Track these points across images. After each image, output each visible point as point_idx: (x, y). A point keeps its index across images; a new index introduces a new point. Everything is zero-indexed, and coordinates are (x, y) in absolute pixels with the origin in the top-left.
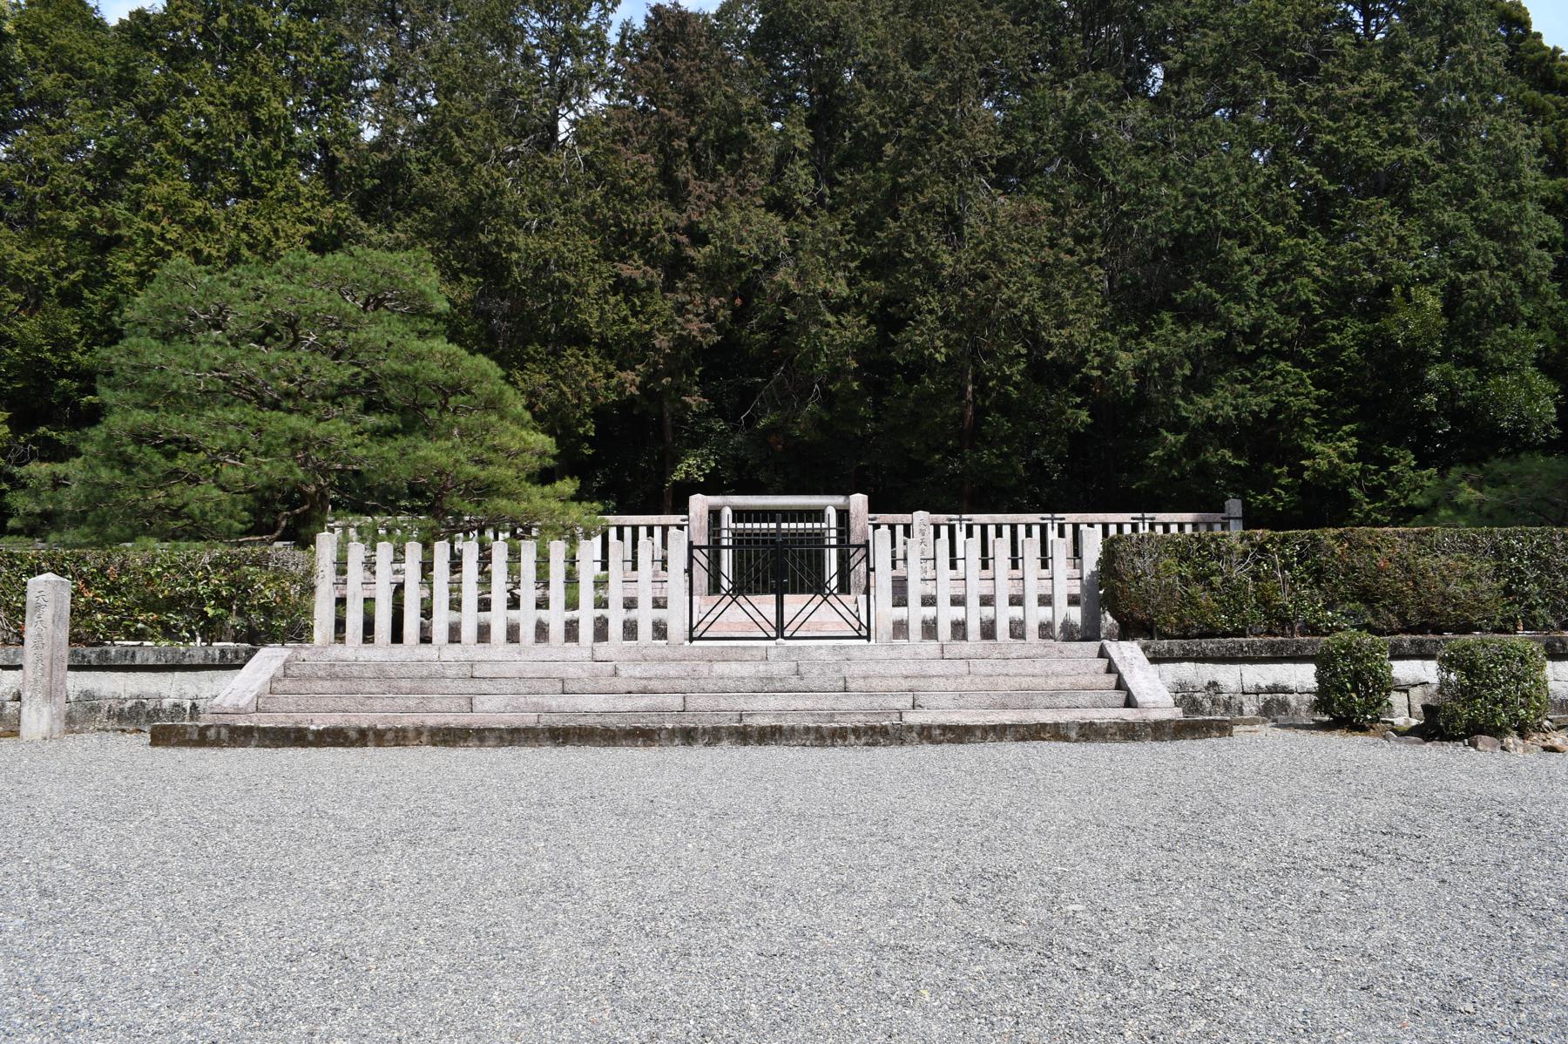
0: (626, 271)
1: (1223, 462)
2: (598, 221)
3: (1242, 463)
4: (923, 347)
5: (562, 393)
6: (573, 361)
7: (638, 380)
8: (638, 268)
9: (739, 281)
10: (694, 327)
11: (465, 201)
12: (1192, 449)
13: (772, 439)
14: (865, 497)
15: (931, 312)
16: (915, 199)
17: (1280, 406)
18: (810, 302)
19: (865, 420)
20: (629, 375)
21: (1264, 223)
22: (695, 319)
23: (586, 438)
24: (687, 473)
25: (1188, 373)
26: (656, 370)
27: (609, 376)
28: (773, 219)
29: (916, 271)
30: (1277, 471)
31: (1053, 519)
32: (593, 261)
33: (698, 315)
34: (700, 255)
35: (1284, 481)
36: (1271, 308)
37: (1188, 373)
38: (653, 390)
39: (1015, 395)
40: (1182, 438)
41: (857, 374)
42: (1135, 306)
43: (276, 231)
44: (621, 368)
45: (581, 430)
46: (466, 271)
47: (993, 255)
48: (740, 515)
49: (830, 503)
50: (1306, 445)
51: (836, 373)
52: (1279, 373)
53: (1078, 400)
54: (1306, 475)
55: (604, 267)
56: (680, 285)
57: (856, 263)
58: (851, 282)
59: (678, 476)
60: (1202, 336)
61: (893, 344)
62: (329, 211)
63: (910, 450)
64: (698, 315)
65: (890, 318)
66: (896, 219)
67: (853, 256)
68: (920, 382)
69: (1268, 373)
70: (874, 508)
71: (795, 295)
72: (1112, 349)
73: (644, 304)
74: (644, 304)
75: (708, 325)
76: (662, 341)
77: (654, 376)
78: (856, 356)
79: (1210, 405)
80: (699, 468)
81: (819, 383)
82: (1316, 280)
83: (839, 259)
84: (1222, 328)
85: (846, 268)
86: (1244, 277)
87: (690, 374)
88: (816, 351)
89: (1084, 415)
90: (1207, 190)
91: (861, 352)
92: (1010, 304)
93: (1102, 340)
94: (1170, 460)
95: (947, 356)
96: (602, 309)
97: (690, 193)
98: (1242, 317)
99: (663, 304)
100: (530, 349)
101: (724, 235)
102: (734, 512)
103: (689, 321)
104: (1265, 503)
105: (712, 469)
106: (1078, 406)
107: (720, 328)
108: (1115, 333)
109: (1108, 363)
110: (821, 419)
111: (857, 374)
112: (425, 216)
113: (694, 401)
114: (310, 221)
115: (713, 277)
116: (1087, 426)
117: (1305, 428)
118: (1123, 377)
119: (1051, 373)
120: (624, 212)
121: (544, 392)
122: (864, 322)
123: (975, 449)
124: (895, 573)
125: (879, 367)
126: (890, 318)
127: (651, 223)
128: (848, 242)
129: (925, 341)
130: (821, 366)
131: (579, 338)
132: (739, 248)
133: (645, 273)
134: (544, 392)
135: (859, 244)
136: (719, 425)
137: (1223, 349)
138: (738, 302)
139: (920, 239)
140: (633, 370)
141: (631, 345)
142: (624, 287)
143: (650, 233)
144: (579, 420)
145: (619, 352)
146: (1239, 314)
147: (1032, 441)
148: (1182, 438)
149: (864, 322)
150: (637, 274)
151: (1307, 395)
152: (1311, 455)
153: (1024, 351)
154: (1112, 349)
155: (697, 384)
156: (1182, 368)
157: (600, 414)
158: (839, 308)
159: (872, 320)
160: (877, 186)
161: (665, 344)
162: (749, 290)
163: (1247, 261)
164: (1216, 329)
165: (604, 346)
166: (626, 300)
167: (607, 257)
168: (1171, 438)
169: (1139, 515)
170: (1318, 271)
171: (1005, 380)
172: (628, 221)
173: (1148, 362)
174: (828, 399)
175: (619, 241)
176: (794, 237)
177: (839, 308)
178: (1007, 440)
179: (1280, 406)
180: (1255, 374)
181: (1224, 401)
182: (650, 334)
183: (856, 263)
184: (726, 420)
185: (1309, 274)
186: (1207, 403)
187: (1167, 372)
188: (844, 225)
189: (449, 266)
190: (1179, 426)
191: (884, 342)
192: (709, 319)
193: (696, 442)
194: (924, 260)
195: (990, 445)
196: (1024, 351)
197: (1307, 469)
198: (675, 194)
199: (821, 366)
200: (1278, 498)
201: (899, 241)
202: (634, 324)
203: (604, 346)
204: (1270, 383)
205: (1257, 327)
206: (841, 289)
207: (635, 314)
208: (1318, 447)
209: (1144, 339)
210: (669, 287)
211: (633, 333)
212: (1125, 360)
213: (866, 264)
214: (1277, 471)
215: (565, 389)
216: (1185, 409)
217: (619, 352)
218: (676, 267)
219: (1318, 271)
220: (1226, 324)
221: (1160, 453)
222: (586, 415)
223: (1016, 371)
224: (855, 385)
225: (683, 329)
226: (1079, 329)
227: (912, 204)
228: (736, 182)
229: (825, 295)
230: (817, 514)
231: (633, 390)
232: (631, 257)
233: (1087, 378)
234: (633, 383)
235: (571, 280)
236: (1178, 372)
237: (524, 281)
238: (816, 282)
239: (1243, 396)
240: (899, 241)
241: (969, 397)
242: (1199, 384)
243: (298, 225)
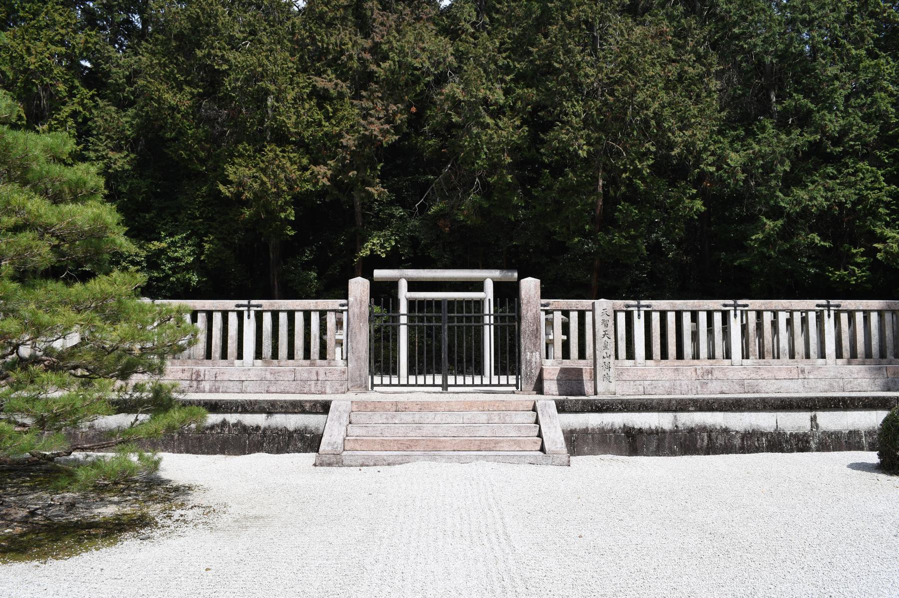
0: (320, 83)
1: (812, 245)
2: (297, 42)
3: (827, 244)
4: (568, 143)
5: (263, 183)
6: (271, 155)
7: (329, 173)
8: (330, 81)
9: (414, 90)
10: (376, 128)
11: (186, 24)
12: (786, 234)
13: (441, 223)
14: (538, 281)
15: (576, 115)
16: (563, 18)
17: (862, 199)
18: (472, 106)
19: (517, 207)
20: (322, 169)
21: (849, 47)
22: (373, 121)
23: (287, 221)
24: (371, 250)
25: (788, 169)
26: (344, 166)
27: (304, 169)
28: (444, 40)
29: (564, 79)
30: (854, 251)
31: (735, 306)
32: (292, 74)
33: (379, 119)
34: (381, 70)
35: (859, 260)
36: (856, 118)
37: (788, 169)
38: (342, 181)
39: (642, 187)
40: (780, 223)
41: (511, 168)
42: (742, 118)
43: (28, 49)
44: (316, 164)
45: (283, 215)
46: (189, 83)
47: (629, 67)
48: (414, 286)
49: (489, 276)
50: (879, 231)
51: (494, 167)
52: (860, 170)
53: (694, 191)
54: (879, 256)
55: (301, 79)
56: (364, 93)
57: (511, 76)
58: (507, 92)
59: (365, 253)
60: (800, 139)
61: (543, 142)
62: (81, 37)
63: (555, 233)
64: (379, 119)
65: (539, 121)
66: (546, 36)
67: (507, 69)
68: (565, 175)
69: (851, 170)
70: (546, 293)
71: (460, 101)
72: (723, 149)
73: (335, 111)
74: (334, 112)
75: (387, 126)
76: (349, 140)
77: (344, 169)
78: (511, 153)
79: (806, 197)
80: (382, 246)
81: (480, 177)
82: (891, 95)
83: (495, 73)
84: (816, 132)
85: (502, 81)
86: (834, 91)
87: (373, 169)
88: (477, 150)
89: (699, 205)
90: (806, 15)
91: (515, 149)
92: (644, 106)
93: (715, 142)
94: (767, 242)
95: (588, 152)
96: (298, 112)
97: (374, 20)
98: (833, 123)
99: (350, 111)
100: (240, 147)
101: (401, 51)
102: (408, 282)
103: (371, 123)
104: (842, 278)
105: (393, 247)
106: (693, 198)
107: (397, 130)
108: (724, 136)
109: (720, 162)
110: (481, 207)
111: (511, 168)
112: (157, 39)
113: (376, 190)
114: (62, 43)
115: (392, 89)
116: (700, 215)
117: (877, 216)
118: (732, 173)
119: (672, 170)
120: (319, 34)
121: (249, 181)
122: (518, 123)
123: (607, 232)
124: (567, 364)
125: (529, 163)
126: (539, 121)
127: (342, 44)
128: (505, 58)
129: (570, 139)
130: (481, 162)
131: (281, 138)
132: (414, 61)
133: (336, 85)
134: (249, 181)
135: (513, 61)
136: (399, 212)
137: (815, 148)
138: (414, 110)
139: (568, 52)
140: (326, 165)
141: (324, 144)
142: (321, 97)
143: (342, 52)
144: (281, 207)
145: (316, 151)
146: (830, 121)
147: (652, 226)
148: (780, 223)
149: (518, 123)
150: (329, 86)
151: (880, 190)
152: (883, 239)
153: (653, 149)
154: (723, 149)
155: (378, 177)
156: (782, 164)
157: (299, 201)
158: (498, 112)
159: (524, 122)
160: (529, 13)
161: (351, 143)
162: (424, 102)
163: (836, 77)
164: (811, 134)
165: (302, 145)
166: (320, 107)
167: (305, 70)
168: (770, 224)
169: (824, 302)
170: (891, 88)
171: (637, 172)
172: (322, 41)
173: (751, 161)
174: (487, 190)
175: (314, 58)
176: (460, 56)
177: (498, 112)
178: (635, 224)
179: (862, 199)
180: (840, 172)
181: (814, 195)
182: (340, 135)
183: (511, 76)
184: (404, 208)
185: (883, 89)
186: (802, 194)
187: (768, 169)
188: (501, 44)
189: (175, 79)
190: (776, 212)
191: (535, 140)
192: (388, 122)
193: (381, 226)
194: (570, 70)
195: (619, 228)
196: (653, 149)
197: (880, 251)
198: (364, 26)
199: (481, 162)
200: (853, 273)
201: (550, 54)
202: (327, 127)
203: (302, 145)
204: (853, 179)
205: (844, 132)
206: (498, 96)
207: (328, 118)
208: (888, 232)
209: (750, 141)
210: (357, 96)
211: (326, 134)
212: (735, 159)
213: (520, 78)
214: (854, 251)
215: (265, 179)
216: (784, 201)
217: (316, 151)
218: (362, 81)
219: (891, 88)
220: (822, 129)
221: (760, 236)
222: (286, 203)
223: (646, 167)
224: (509, 178)
225: (366, 130)
226: (698, 129)
227: (561, 22)
228: (412, 12)
229: (485, 101)
230: (478, 286)
231: (325, 181)
232: (325, 72)
233: (703, 175)
234: (325, 175)
235: (272, 88)
236: (780, 168)
237: (234, 89)
238: (478, 90)
239: (832, 190)
240: (550, 54)
241: (600, 190)
242: (790, 181)
243: (50, 46)
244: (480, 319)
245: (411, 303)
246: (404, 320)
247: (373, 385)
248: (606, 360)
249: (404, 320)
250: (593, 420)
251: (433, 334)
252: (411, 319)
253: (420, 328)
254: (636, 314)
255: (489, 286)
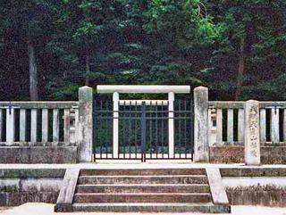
48: (123, 96)
49: (172, 90)
230: (164, 96)
244: (166, 115)
245: (121, 107)
246: (116, 115)
247: (95, 159)
248: (254, 141)
249: (116, 115)
250: (246, 182)
251: (135, 124)
252: (175, 115)
253: (154, 121)
254: (273, 110)
255: (171, 98)
